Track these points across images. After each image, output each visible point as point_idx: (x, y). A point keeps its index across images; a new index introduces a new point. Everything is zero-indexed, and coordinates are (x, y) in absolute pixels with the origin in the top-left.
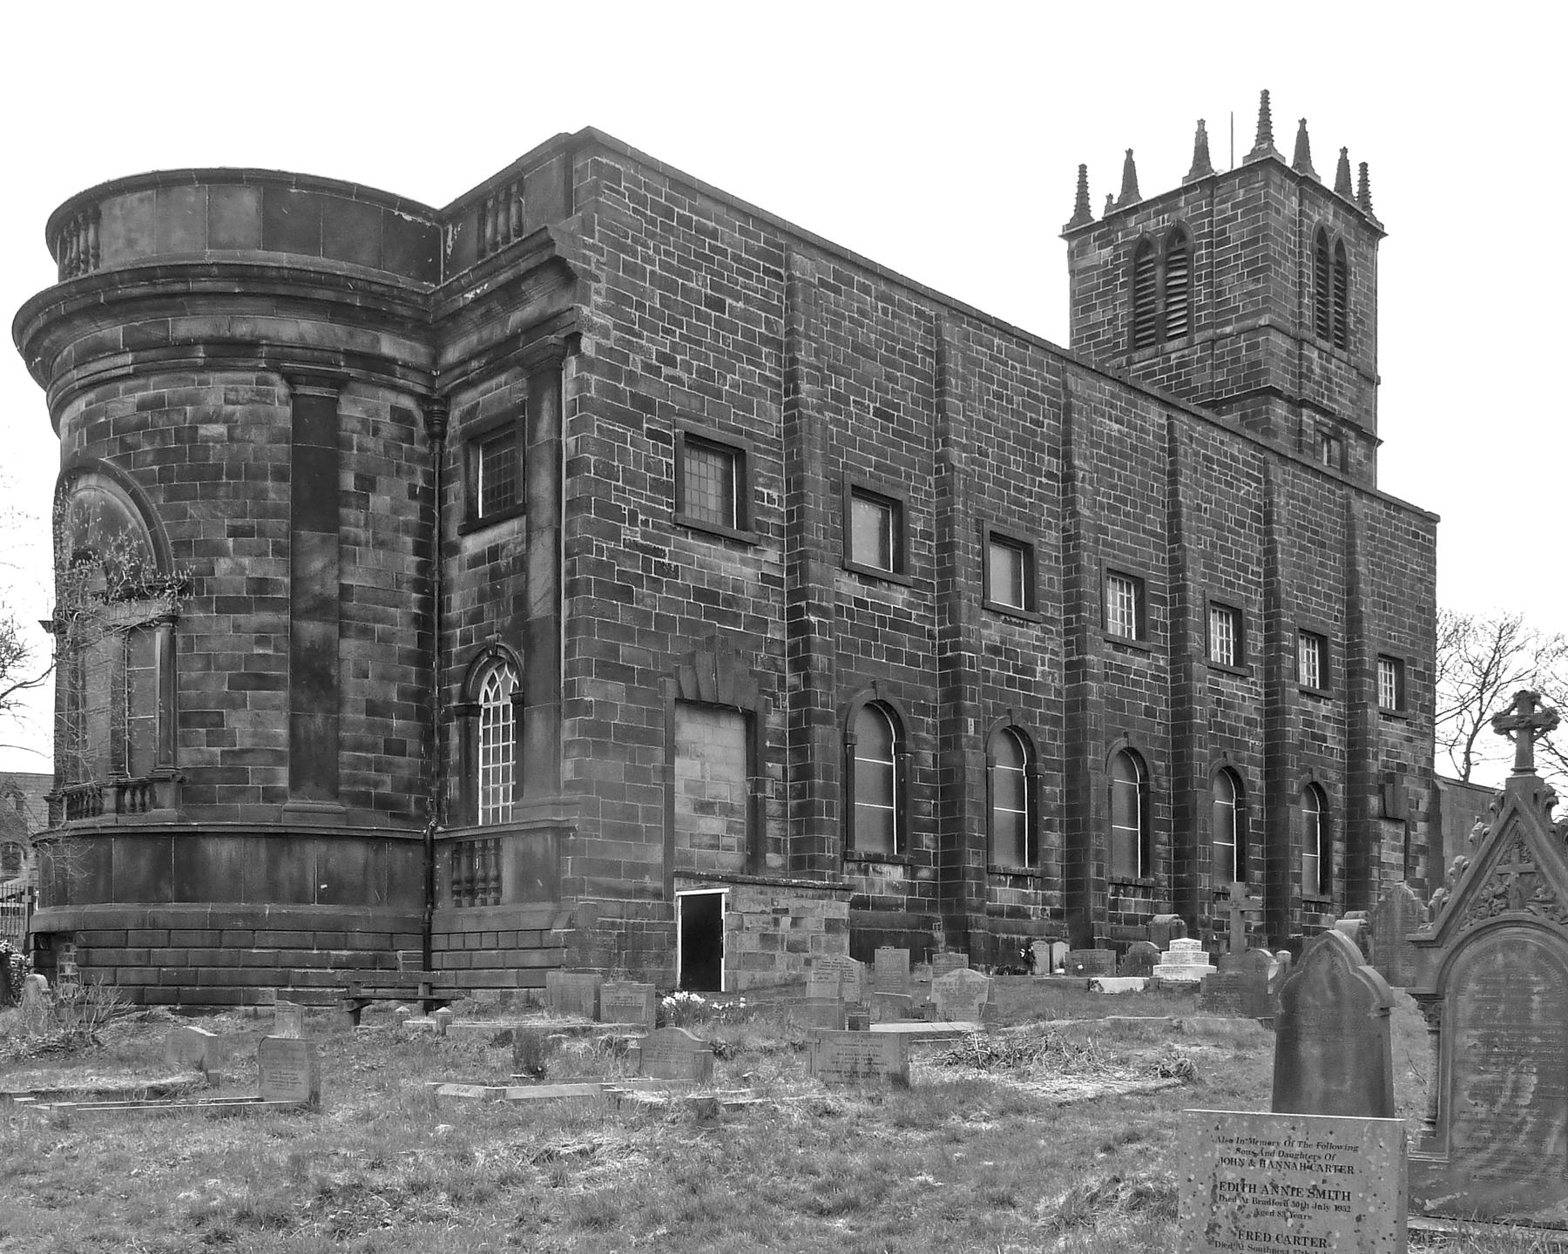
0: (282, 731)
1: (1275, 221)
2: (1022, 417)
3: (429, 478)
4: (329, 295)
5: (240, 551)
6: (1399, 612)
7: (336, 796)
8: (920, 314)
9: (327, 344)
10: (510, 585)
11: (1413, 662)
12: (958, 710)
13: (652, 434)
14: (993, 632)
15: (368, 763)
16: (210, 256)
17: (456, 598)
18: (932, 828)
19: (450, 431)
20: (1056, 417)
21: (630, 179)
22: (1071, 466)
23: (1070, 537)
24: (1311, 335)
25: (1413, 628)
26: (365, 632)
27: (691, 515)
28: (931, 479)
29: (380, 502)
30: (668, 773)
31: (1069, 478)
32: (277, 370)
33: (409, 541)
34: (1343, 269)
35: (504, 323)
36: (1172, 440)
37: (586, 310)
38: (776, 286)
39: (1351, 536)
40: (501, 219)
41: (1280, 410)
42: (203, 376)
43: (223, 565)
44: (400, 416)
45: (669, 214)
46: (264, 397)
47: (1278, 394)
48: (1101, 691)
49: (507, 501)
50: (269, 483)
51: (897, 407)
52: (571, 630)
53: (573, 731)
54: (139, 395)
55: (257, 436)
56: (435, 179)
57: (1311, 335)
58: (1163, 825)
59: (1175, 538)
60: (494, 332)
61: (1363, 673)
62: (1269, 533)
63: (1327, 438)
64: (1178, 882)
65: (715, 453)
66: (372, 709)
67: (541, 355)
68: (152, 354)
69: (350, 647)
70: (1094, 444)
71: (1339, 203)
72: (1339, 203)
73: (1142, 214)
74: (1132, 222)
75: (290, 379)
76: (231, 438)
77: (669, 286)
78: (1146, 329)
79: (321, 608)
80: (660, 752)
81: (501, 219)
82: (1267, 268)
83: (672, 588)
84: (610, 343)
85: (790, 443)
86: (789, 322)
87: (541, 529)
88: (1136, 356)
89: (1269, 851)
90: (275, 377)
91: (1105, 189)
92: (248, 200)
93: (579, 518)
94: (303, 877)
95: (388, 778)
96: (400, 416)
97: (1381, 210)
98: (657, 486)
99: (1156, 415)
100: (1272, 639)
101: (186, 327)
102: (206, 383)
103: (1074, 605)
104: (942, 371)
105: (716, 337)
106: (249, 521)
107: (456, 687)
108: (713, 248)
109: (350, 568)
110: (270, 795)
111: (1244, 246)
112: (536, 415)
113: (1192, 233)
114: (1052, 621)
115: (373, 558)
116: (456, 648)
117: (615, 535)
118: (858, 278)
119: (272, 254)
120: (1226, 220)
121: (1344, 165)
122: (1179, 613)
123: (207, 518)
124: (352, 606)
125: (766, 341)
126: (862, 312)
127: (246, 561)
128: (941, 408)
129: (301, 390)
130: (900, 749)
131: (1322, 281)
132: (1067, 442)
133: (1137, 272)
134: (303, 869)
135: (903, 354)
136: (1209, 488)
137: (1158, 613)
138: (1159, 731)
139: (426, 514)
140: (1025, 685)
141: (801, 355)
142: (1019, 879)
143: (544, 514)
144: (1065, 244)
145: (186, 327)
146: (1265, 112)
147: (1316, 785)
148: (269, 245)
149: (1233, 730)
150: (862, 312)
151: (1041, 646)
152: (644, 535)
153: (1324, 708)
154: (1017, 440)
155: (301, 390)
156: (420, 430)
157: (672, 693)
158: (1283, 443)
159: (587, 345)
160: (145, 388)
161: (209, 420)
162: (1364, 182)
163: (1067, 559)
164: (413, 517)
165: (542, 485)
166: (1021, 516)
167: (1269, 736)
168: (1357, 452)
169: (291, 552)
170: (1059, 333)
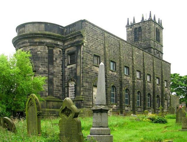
0: (47, 88)
1: (152, 27)
2: (128, 52)
3: (63, 58)
4: (53, 37)
5: (42, 67)
6: (167, 75)
7: (53, 96)
8: (117, 40)
9: (52, 43)
10: (74, 72)
11: (168, 81)
12: (122, 87)
13: (91, 54)
14: (125, 77)
15: (57, 92)
16: (39, 32)
17: (66, 73)
18: (119, 100)
19: (65, 53)
20: (131, 52)
21: (89, 25)
22: (133, 58)
23: (133, 66)
24: (156, 41)
25: (168, 77)
26: (56, 77)
27: (94, 64)
28: (119, 60)
29: (58, 61)
30: (92, 94)
31: (133, 59)
32: (46, 46)
33: (61, 66)
34: (159, 33)
35: (73, 41)
36: (143, 55)
37: (84, 40)
38: (103, 37)
39: (162, 66)
40: (72, 28)
41: (152, 50)
42: (38, 46)
43: (40, 69)
44: (60, 51)
45: (92, 29)
46: (45, 49)
47: (152, 48)
48: (136, 85)
49: (73, 62)
50: (45, 59)
51: (115, 51)
52: (82, 77)
53: (83, 89)
54: (30, 48)
55: (44, 53)
56: (64, 23)
57: (156, 41)
58: (142, 100)
59: (144, 66)
60: (72, 42)
61: (163, 82)
62: (153, 66)
63: (157, 53)
64: (144, 107)
65: (97, 57)
66: (57, 86)
67: (79, 45)
68: (31, 43)
69: (55, 79)
70: (135, 55)
71: (159, 25)
72: (159, 25)
73: (136, 25)
74: (134, 26)
75: (48, 47)
76: (41, 54)
77: (92, 37)
78: (136, 39)
79: (52, 74)
80: (92, 91)
81: (72, 28)
82: (151, 33)
83: (93, 73)
84: (86, 44)
85: (105, 55)
86: (104, 41)
87: (78, 65)
88: (135, 42)
89: (153, 103)
90: (46, 46)
91: (131, 21)
92: (43, 25)
93: (83, 64)
94: (50, 106)
95: (59, 94)
96: (60, 51)
97: (163, 26)
98: (91, 60)
99: (141, 52)
100: (154, 78)
101: (36, 40)
102: (38, 47)
103: (133, 75)
104: (120, 47)
105: (97, 43)
106: (43, 63)
107: (66, 84)
108: (97, 33)
109: (54, 69)
110: (46, 96)
111: (148, 30)
112: (78, 52)
113: (142, 28)
114: (131, 76)
115: (57, 68)
116: (66, 79)
117: (87, 66)
118: (111, 36)
119: (46, 32)
120: (146, 26)
121: (159, 20)
122: (144, 75)
123: (39, 63)
124: (55, 74)
125: (102, 44)
126: (111, 40)
127: (43, 68)
128: (120, 51)
129: (49, 48)
130: (115, 91)
131: (157, 35)
132: (132, 55)
133: (135, 32)
134: (50, 105)
135: (116, 45)
136: (147, 60)
137: (142, 75)
138: (142, 89)
139: (63, 63)
140: (128, 84)
141: (106, 45)
142: (128, 107)
143: (79, 64)
144: (126, 28)
145: (36, 40)
146: (150, 14)
147: (158, 95)
148: (46, 30)
149: (149, 89)
150: (111, 40)
151: (130, 79)
152: (90, 66)
153: (159, 86)
154: (127, 55)
155: (49, 48)
156: (62, 53)
157: (93, 85)
158: (152, 54)
159: (84, 44)
160: (30, 47)
161: (38, 51)
162: (161, 22)
163: (133, 69)
164: (61, 63)
165: (79, 60)
166: (128, 64)
167: (153, 90)
168: (161, 55)
169: (48, 67)
170: (125, 39)
